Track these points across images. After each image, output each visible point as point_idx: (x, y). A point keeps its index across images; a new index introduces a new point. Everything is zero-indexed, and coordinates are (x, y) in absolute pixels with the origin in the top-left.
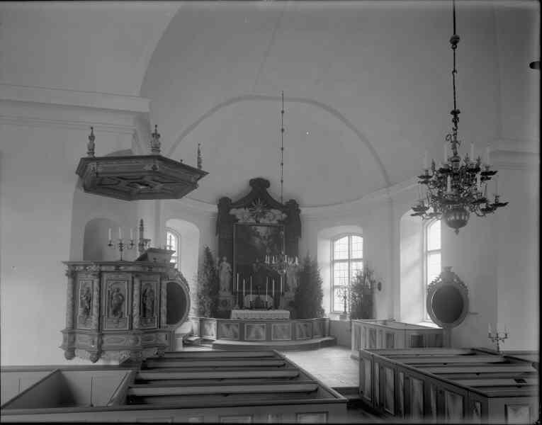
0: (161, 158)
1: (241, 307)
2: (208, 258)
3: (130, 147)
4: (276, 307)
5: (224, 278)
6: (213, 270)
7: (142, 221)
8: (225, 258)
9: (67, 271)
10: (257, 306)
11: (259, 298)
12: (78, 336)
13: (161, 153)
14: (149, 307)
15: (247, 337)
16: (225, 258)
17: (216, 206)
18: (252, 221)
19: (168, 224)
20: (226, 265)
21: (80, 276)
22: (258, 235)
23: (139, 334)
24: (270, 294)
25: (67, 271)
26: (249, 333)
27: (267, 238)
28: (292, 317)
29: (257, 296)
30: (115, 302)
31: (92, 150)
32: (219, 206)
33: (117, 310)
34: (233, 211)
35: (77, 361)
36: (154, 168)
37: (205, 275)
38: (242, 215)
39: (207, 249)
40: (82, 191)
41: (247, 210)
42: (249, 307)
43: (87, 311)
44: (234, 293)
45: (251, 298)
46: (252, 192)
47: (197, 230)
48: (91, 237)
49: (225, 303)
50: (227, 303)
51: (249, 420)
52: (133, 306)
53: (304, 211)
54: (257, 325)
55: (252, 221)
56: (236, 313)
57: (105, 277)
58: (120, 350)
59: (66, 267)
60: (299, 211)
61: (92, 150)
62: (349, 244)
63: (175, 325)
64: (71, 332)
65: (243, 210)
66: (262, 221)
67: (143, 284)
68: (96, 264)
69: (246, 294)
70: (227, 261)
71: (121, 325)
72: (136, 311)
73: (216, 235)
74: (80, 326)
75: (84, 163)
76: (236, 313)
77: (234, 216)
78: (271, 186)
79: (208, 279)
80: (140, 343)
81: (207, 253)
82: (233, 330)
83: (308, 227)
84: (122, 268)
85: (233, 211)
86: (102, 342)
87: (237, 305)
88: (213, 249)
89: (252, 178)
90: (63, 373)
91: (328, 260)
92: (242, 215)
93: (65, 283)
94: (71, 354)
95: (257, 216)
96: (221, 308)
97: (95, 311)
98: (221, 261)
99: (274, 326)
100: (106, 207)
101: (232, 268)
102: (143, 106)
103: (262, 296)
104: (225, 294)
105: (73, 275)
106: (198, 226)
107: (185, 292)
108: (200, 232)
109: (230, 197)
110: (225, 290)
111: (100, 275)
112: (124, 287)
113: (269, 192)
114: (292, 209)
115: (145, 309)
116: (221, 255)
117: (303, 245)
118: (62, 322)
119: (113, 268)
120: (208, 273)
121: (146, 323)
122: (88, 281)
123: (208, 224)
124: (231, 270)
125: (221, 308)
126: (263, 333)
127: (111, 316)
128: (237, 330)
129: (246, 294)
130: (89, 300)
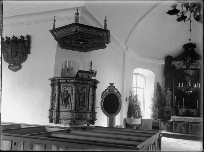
1: (177, 114)
2: (158, 88)
7: (91, 61)
8: (168, 88)
11: (188, 110)
12: (61, 113)
13: (79, 22)
15: (175, 130)
16: (168, 88)
17: (164, 61)
18: (184, 67)
20: (169, 92)
22: (188, 75)
23: (74, 112)
24: (195, 108)
26: (176, 128)
27: (194, 76)
29: (187, 109)
31: (54, 26)
32: (165, 61)
33: (66, 101)
34: (173, 63)
36: (76, 30)
37: (157, 97)
38: (178, 64)
39: (158, 83)
41: (182, 62)
42: (182, 115)
45: (183, 110)
46: (185, 51)
47: (154, 74)
50: (169, 113)
51: (81, 150)
55: (184, 67)
58: (67, 119)
59: (50, 82)
61: (54, 26)
62: (16, 16)
63: (113, 115)
65: (179, 62)
66: (191, 67)
67: (79, 89)
70: (170, 90)
71: (68, 107)
73: (164, 76)
76: (173, 118)
77: (174, 65)
78: (196, 48)
79: (157, 99)
80: (74, 116)
81: (158, 87)
82: (167, 126)
84: (68, 81)
85: (173, 63)
86: (59, 115)
87: (175, 114)
88: (162, 82)
89: (184, 43)
90: (46, 128)
92: (178, 64)
93: (50, 88)
94: (51, 121)
95: (188, 65)
96: (165, 115)
98: (166, 90)
99: (191, 125)
101: (172, 93)
104: (168, 107)
105: (53, 85)
107: (119, 98)
108: (155, 75)
110: (168, 105)
112: (69, 89)
116: (166, 87)
119: (65, 81)
120: (158, 95)
121: (80, 108)
123: (160, 70)
124: (172, 94)
125: (165, 115)
126: (184, 129)
127: (64, 103)
128: (169, 126)
129: (181, 108)
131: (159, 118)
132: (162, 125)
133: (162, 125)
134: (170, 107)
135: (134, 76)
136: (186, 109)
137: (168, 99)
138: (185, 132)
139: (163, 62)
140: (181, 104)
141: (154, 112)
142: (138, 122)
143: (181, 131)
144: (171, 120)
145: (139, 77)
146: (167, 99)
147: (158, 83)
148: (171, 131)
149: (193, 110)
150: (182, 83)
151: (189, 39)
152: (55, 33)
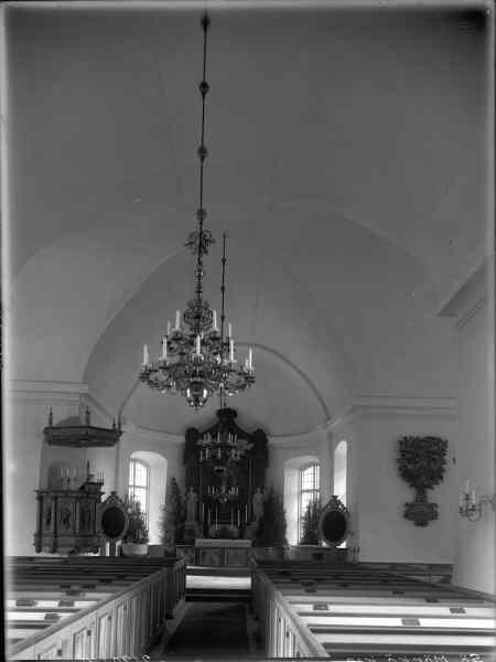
0: (89, 427)
1: (206, 535)
2: (173, 492)
3: (77, 414)
4: (241, 537)
5: (191, 508)
6: (178, 500)
8: (192, 489)
9: (437, 483)
10: (224, 535)
14: (87, 520)
16: (192, 489)
19: (133, 456)
20: (193, 495)
21: (45, 500)
25: (437, 483)
28: (253, 545)
30: (64, 516)
31: (51, 422)
33: (66, 521)
35: (41, 555)
40: (46, 445)
43: (49, 522)
44: (200, 523)
45: (217, 527)
47: (163, 460)
48: (52, 473)
49: (192, 532)
52: (76, 520)
53: (271, 440)
54: (210, 551)
56: (200, 542)
57: (59, 499)
60: (267, 440)
64: (39, 535)
68: (54, 492)
69: (212, 523)
70: (194, 491)
72: (78, 522)
74: (44, 532)
75: (46, 430)
76: (200, 542)
83: (276, 456)
91: (295, 490)
93: (36, 502)
94: (39, 551)
97: (52, 521)
100: (63, 453)
102: (85, 389)
103: (228, 526)
104: (191, 523)
105: (40, 499)
106: (164, 455)
109: (197, 427)
111: (56, 498)
112: (71, 509)
113: (239, 425)
114: (259, 439)
115: (84, 522)
116: (188, 485)
117: (270, 474)
118: (34, 529)
122: (49, 502)
123: (177, 452)
125: (186, 537)
126: (216, 559)
129: (212, 523)
130: (50, 514)
131: (177, 542)
132: (180, 553)
133: (180, 553)
134: (193, 523)
135: (131, 466)
136: (221, 526)
137: (191, 508)
138: (217, 564)
139: (182, 439)
140: (213, 517)
141: (167, 532)
142: (143, 550)
143: (212, 563)
144: (197, 544)
145: (138, 466)
146: (189, 507)
147: (174, 479)
148: (196, 565)
149: (232, 528)
150: (146, 349)
151: (194, 227)
152: (244, 551)
